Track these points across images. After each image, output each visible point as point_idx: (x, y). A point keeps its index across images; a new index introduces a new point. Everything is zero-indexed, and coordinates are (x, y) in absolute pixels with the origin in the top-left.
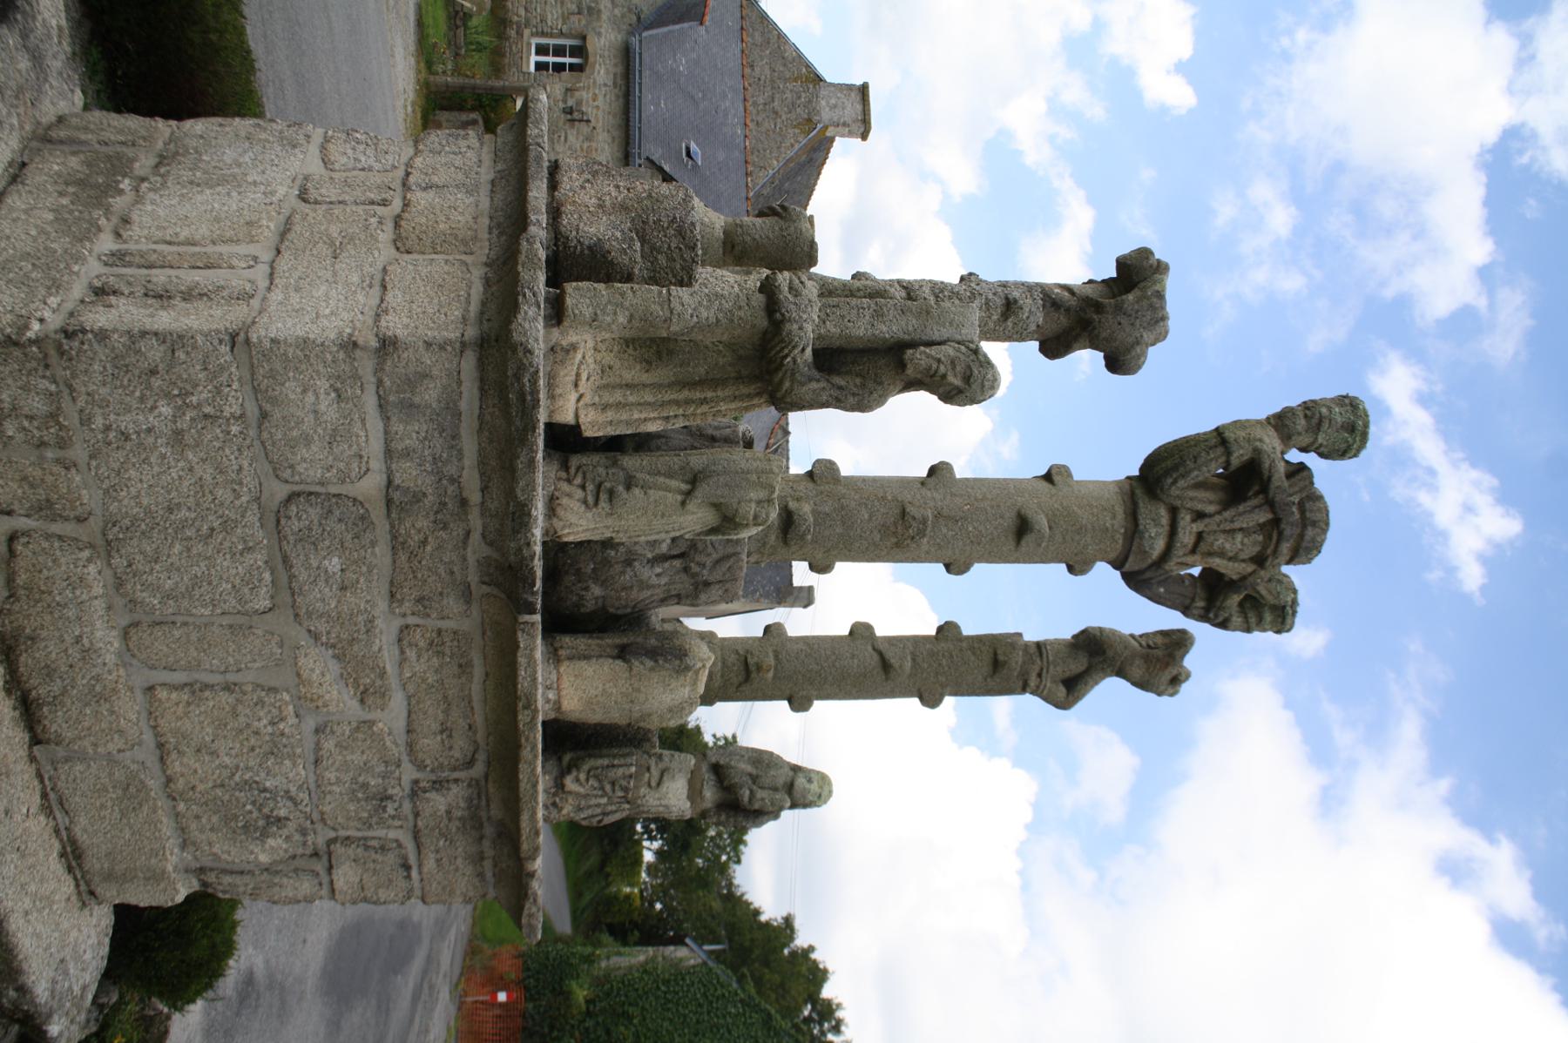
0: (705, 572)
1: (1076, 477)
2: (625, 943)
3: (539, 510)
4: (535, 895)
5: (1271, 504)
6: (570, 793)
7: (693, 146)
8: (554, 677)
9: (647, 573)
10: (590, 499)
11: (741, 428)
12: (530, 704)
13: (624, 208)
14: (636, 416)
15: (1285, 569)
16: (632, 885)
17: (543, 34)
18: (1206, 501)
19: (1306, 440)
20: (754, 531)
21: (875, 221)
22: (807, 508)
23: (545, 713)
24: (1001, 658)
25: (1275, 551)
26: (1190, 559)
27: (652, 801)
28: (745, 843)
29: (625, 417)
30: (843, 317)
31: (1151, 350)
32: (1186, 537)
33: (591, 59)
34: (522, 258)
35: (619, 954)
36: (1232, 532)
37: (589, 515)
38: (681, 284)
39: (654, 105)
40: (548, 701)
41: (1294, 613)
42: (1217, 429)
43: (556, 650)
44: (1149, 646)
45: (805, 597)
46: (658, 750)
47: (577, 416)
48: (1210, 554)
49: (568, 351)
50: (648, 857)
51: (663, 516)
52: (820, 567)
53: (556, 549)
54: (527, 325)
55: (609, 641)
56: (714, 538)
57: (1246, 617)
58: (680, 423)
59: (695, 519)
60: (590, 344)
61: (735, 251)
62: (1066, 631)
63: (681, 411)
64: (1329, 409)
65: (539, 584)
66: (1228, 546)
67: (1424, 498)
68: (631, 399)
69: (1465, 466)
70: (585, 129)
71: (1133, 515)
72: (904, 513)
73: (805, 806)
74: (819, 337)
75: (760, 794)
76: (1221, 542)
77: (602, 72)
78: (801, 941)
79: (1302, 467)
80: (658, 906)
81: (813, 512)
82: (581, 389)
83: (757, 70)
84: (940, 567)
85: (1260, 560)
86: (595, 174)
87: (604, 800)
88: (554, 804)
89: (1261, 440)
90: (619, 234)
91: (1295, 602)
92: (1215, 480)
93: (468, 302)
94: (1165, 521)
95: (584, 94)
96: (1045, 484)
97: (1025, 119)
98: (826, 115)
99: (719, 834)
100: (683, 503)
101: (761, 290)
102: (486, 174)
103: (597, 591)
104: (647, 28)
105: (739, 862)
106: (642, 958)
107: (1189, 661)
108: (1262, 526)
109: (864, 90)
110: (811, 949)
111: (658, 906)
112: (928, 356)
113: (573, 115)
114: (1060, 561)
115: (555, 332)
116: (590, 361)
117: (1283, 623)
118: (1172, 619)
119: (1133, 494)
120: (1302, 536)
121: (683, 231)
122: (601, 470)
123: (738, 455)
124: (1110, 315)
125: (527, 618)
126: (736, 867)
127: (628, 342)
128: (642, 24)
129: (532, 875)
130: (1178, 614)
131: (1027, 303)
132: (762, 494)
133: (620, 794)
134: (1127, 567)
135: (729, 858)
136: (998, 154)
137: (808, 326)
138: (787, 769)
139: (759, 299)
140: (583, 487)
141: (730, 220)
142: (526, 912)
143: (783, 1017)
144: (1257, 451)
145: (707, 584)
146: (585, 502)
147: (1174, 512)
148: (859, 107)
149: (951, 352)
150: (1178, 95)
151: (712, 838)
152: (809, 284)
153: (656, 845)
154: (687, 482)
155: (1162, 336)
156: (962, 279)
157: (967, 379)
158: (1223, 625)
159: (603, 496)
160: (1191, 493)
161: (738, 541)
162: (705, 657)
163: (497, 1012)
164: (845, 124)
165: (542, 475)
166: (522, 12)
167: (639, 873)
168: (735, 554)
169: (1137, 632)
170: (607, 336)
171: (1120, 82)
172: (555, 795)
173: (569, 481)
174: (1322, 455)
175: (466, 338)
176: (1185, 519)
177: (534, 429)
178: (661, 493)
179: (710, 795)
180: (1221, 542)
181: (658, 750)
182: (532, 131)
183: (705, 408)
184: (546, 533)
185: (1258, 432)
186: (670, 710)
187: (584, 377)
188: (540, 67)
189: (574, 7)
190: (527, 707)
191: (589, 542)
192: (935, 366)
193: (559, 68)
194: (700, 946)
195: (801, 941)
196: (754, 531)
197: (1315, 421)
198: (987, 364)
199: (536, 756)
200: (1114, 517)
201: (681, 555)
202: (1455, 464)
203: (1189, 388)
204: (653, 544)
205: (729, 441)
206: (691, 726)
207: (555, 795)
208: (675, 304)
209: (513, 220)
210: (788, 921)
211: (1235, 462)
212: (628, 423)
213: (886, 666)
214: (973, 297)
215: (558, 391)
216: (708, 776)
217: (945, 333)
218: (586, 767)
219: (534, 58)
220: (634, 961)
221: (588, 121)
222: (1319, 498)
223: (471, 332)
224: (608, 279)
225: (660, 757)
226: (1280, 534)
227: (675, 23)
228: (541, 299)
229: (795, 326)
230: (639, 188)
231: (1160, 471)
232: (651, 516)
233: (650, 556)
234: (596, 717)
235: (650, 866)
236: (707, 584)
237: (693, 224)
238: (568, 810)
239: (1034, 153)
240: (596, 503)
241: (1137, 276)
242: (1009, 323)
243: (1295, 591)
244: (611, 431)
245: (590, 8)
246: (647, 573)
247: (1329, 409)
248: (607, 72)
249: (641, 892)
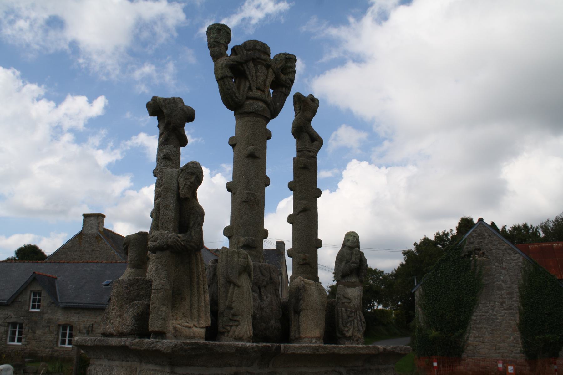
0: (266, 279)
1: (234, 135)
2: (414, 316)
3: (239, 344)
4: (392, 348)
5: (247, 61)
6: (352, 334)
7: (104, 283)
8: (306, 339)
9: (266, 302)
10: (236, 323)
11: (210, 264)
12: (317, 349)
13: (121, 307)
14: (203, 304)
15: (272, 57)
16: (392, 314)
17: (57, 341)
18: (244, 86)
19: (223, 48)
20: (250, 259)
21: (132, 210)
22: (242, 239)
23: (321, 343)
24: (303, 166)
25: (265, 61)
26: (267, 93)
27: (356, 302)
28: (376, 269)
29: (203, 309)
30: (167, 221)
31: (186, 104)
32: (258, 94)
33: (68, 323)
34: (138, 348)
35: (418, 318)
36: (256, 76)
37: (242, 324)
38: (151, 285)
39: (87, 298)
40: (316, 342)
41: (288, 54)
42: (217, 81)
43: (296, 339)
44: (300, 110)
45: (281, 244)
46: (336, 299)
47: (202, 328)
48: (265, 85)
49: (176, 331)
50: (380, 307)
51: (243, 295)
52: (265, 234)
53: (255, 338)
54: (165, 346)
55: (293, 317)
56: (252, 276)
57: (290, 73)
58: (207, 287)
59: (245, 282)
60: (174, 321)
61: (141, 264)
62: (293, 141)
63: (202, 286)
64: (211, 38)
65: (269, 344)
66: (262, 78)
67: (254, 22)
68: (196, 306)
69: (243, 7)
70: (96, 326)
71: (249, 114)
72: (245, 202)
73: (358, 242)
74: (174, 231)
75: (353, 260)
76: (260, 81)
77: (74, 318)
78: (413, 248)
79: (233, 49)
80: (400, 303)
81: (244, 236)
82: (192, 325)
84: (267, 188)
85: (268, 67)
86: (107, 319)
87: (356, 321)
88: (357, 340)
89: (222, 64)
90: (131, 309)
91: (285, 54)
92: (237, 82)
93: (156, 370)
94: (251, 102)
95: (82, 326)
96: (236, 147)
97: (103, 158)
98: (95, 231)
99: (372, 279)
100: (239, 287)
101: (155, 253)
102: (105, 362)
103: (273, 322)
104: (57, 300)
105: (383, 272)
106: (419, 309)
107: (306, 95)
108: (255, 65)
109: (86, 216)
110: (415, 244)
111: (400, 303)
112: (183, 188)
113: (90, 331)
114: (266, 142)
115: (168, 335)
116: (180, 322)
117: (292, 59)
118: (289, 102)
119: (241, 114)
120: (259, 50)
121: (131, 284)
122: (225, 319)
123: (220, 265)
124: (172, 118)
125: (282, 349)
126: (384, 273)
127: (174, 307)
128: (55, 302)
129: (385, 349)
130: (288, 98)
131: (165, 151)
132: (236, 256)
133: (353, 314)
134: (269, 117)
135: (381, 276)
136: (117, 169)
137: (170, 235)
138: (344, 249)
139: (158, 254)
140: (231, 326)
141: (128, 266)
142: (399, 352)
143: (442, 255)
144: (226, 66)
145: (271, 279)
146: (237, 326)
147: (248, 98)
148: (92, 218)
149: (182, 180)
150: (100, 103)
151: (373, 282)
152: (153, 234)
153: (376, 304)
154: (230, 285)
155: (180, 100)
156: (155, 176)
157: (192, 174)
158: (292, 81)
159: (235, 318)
160: (241, 91)
161: (254, 266)
162: (300, 280)
163: (441, 366)
164: (99, 224)
165: (226, 342)
166: (48, 350)
167: (387, 311)
168: (259, 267)
169: (294, 114)
170: (171, 314)
171: (94, 123)
172: (353, 340)
173: (229, 332)
174: (229, 42)
175: (169, 371)
176: (251, 94)
177: (206, 344)
178: (234, 295)
179: (354, 279)
180: (260, 81)
181: (336, 299)
182: (89, 343)
183: (201, 277)
184: (249, 341)
185: (219, 65)
186: (320, 294)
187: (187, 324)
189: (47, 329)
190: (318, 350)
191: (253, 324)
192: (187, 186)
194: (415, 287)
195: (413, 248)
196: (250, 259)
197: (215, 44)
198: (187, 166)
199: (337, 347)
200: (250, 121)
201: (259, 288)
202: (242, 11)
203: (199, 88)
204: (254, 299)
205: (215, 269)
206: (329, 289)
207: (353, 340)
208: (158, 287)
209: (124, 352)
210: (405, 253)
211: (230, 74)
212: (206, 307)
213: (304, 210)
214: (162, 172)
215: (192, 335)
216: (346, 280)
217: (174, 182)
218: (342, 328)
219: (67, 346)
220: (421, 312)
221: (92, 324)
222: (245, 43)
223: (167, 369)
224: (148, 314)
225: (339, 298)
226: (258, 58)
227: (56, 289)
228: (155, 340)
229: (169, 240)
230: (114, 301)
231: (231, 101)
232: (243, 299)
233: (259, 301)
234: (323, 323)
235: (384, 306)
236: (271, 279)
237: (129, 280)
238: (359, 335)
239: (117, 156)
240: (238, 321)
241: (156, 108)
242: (173, 158)
243: (280, 54)
244: (209, 314)
245: (48, 323)
246: (266, 302)
247: (211, 38)
249: (394, 310)
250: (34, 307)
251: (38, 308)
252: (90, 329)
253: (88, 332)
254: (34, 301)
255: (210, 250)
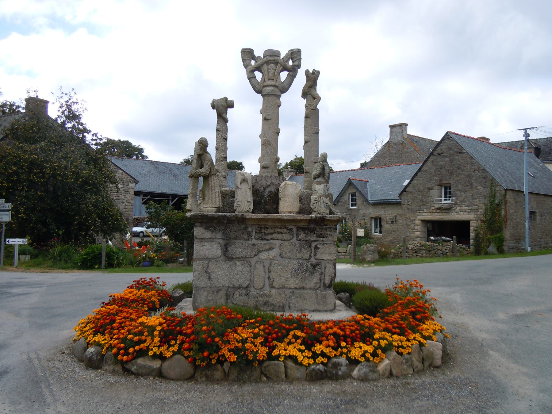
70: (398, 217)
83: (387, 162)
98: (399, 139)
109: (391, 127)
147: (264, 86)
148: (397, 128)
164: (402, 132)
185: (248, 70)
188: (381, 232)
193: (381, 226)
245: (363, 216)
248: (381, 211)
250: (352, 205)
251: (355, 206)
252: (394, 220)
253: (392, 222)
254: (352, 200)
255: (477, 139)
